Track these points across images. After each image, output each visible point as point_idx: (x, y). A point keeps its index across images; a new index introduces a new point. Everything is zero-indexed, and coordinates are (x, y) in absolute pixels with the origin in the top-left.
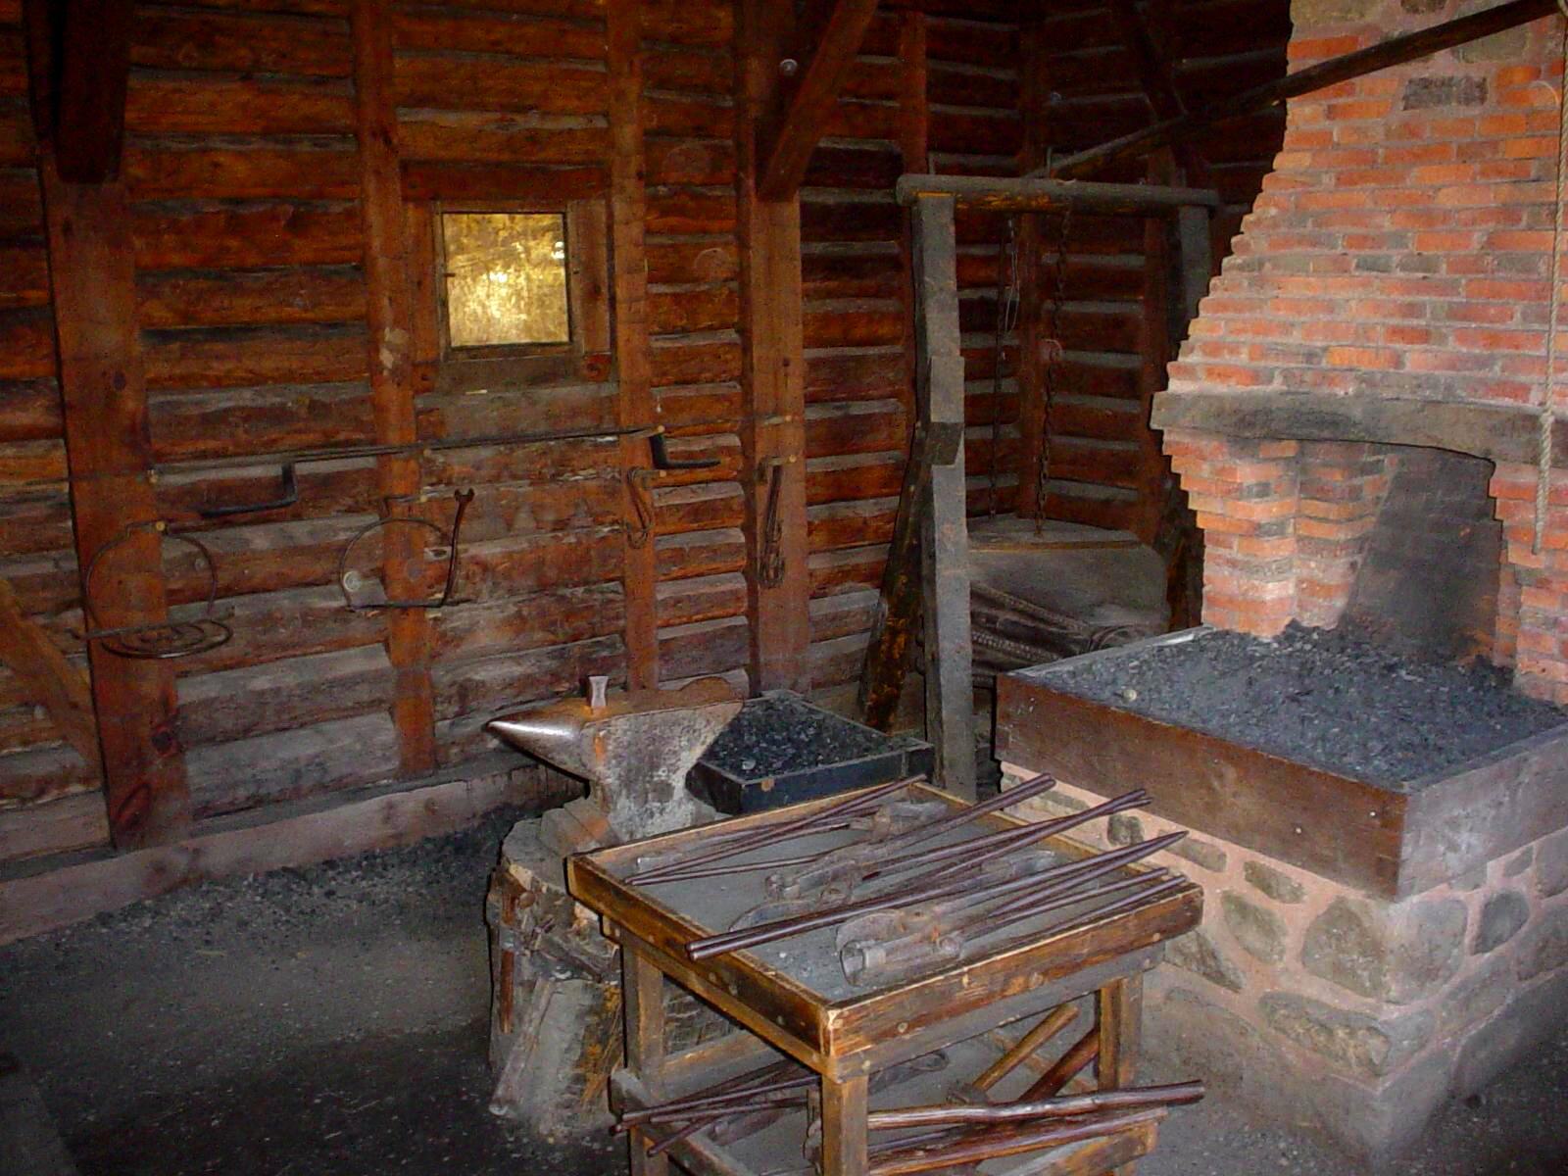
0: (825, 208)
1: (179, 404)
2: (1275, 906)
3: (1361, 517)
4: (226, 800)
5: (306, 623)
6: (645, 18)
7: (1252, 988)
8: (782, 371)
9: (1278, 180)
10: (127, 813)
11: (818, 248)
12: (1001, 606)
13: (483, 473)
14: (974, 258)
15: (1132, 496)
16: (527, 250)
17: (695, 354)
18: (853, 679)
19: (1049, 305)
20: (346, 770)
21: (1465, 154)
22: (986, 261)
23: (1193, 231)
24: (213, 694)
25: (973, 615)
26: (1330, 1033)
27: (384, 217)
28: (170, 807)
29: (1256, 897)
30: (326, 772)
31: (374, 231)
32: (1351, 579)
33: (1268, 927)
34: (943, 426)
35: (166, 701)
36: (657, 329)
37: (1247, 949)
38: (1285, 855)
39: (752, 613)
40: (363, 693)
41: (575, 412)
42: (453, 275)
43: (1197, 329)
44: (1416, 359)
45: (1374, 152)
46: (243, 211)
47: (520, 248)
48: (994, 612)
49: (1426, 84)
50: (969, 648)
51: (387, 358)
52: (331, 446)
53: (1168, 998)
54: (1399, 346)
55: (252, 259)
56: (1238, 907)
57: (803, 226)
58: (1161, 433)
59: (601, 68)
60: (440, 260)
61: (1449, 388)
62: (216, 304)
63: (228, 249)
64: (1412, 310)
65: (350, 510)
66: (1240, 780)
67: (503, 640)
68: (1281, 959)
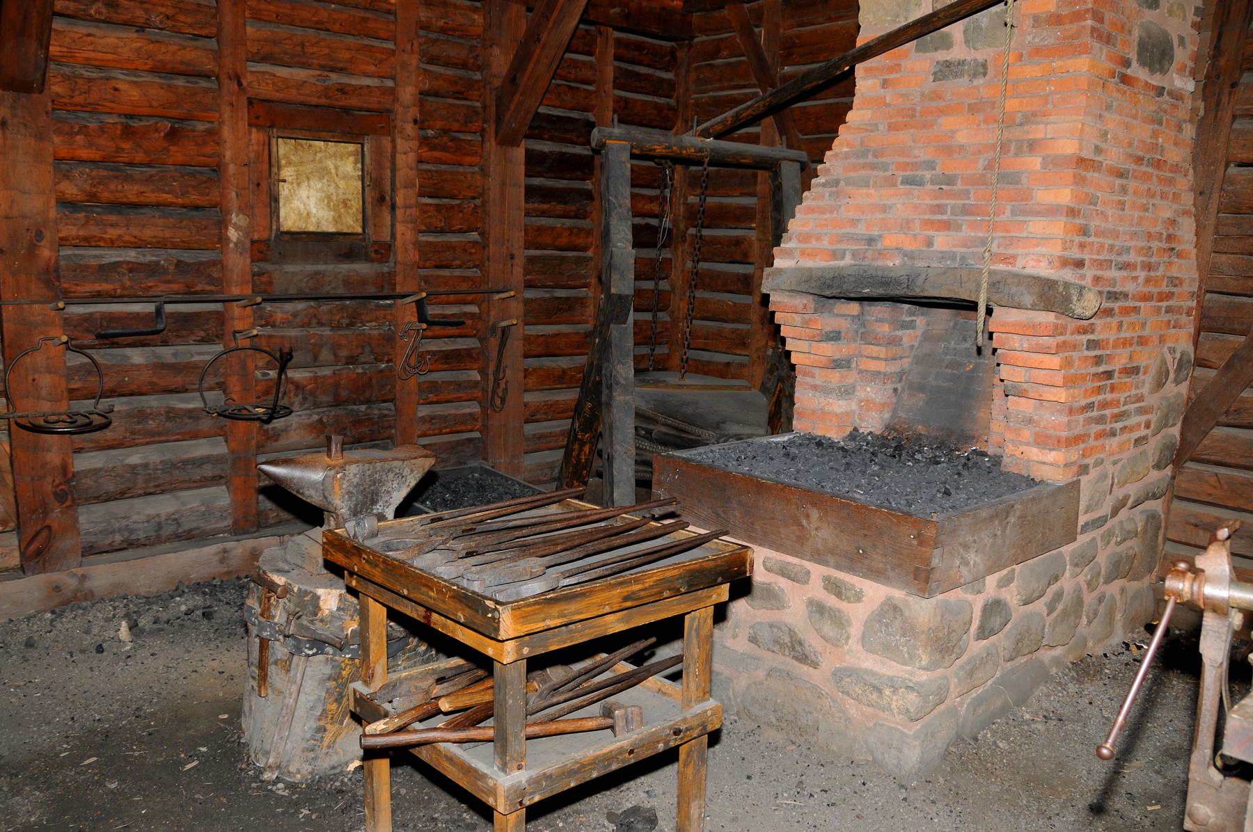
0: (542, 153)
1: (83, 256)
2: (843, 605)
3: (901, 358)
4: (108, 542)
5: (169, 419)
6: (424, 14)
7: (828, 663)
8: (510, 262)
9: (849, 128)
10: (33, 547)
11: (537, 181)
12: (656, 422)
13: (298, 320)
14: (643, 196)
15: (745, 360)
16: (336, 168)
17: (450, 247)
18: (553, 480)
19: (692, 231)
20: (194, 525)
21: (973, 109)
22: (652, 199)
23: (789, 172)
24: (99, 465)
25: (636, 428)
26: (880, 691)
27: (236, 139)
28: (66, 543)
29: (831, 601)
30: (179, 525)
31: (228, 145)
32: (894, 400)
33: (839, 620)
34: (620, 297)
35: (64, 469)
36: (423, 228)
37: (823, 637)
38: (851, 569)
39: (485, 430)
40: (208, 471)
41: (364, 282)
42: (284, 181)
43: (794, 226)
44: (942, 241)
45: (914, 110)
46: (135, 123)
47: (332, 166)
48: (651, 427)
49: (948, 64)
50: (634, 452)
51: (233, 234)
52: (191, 296)
53: (769, 675)
54: (931, 233)
55: (140, 157)
56: (818, 609)
57: (527, 164)
58: (768, 296)
59: (390, 45)
60: (275, 170)
61: (963, 258)
62: (112, 187)
63: (123, 149)
64: (940, 209)
65: (203, 341)
66: (820, 519)
67: (309, 438)
68: (847, 643)
